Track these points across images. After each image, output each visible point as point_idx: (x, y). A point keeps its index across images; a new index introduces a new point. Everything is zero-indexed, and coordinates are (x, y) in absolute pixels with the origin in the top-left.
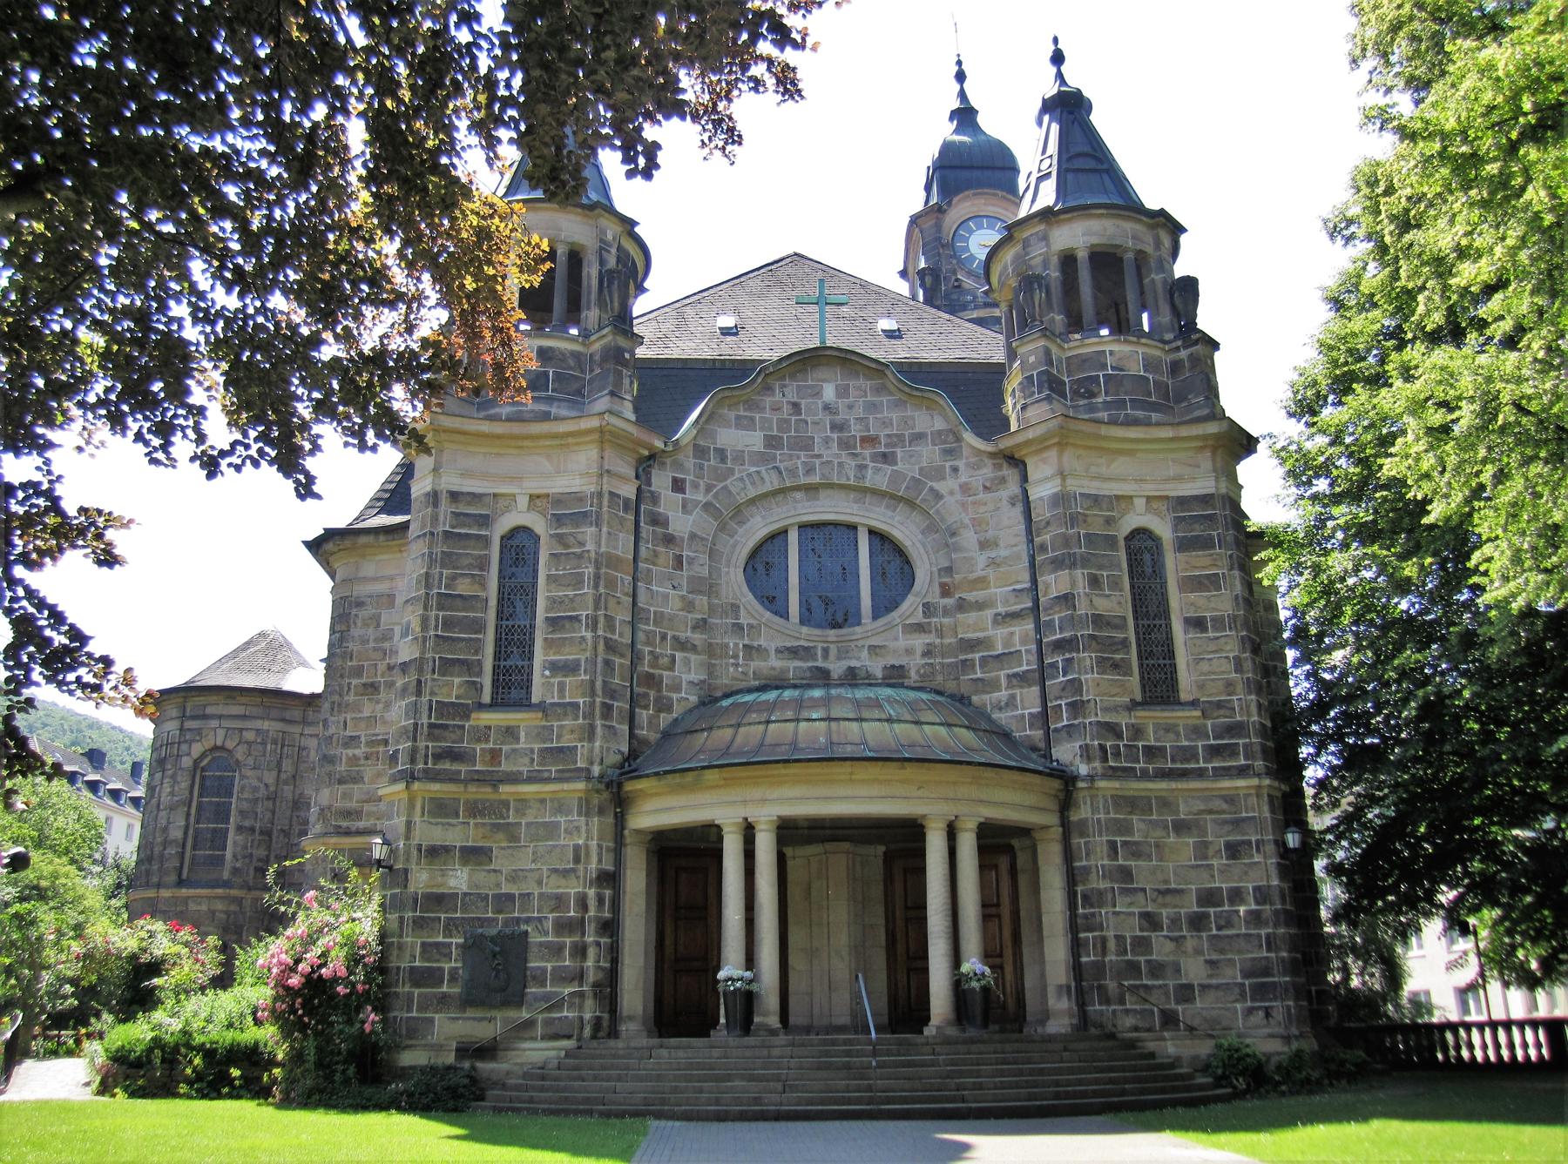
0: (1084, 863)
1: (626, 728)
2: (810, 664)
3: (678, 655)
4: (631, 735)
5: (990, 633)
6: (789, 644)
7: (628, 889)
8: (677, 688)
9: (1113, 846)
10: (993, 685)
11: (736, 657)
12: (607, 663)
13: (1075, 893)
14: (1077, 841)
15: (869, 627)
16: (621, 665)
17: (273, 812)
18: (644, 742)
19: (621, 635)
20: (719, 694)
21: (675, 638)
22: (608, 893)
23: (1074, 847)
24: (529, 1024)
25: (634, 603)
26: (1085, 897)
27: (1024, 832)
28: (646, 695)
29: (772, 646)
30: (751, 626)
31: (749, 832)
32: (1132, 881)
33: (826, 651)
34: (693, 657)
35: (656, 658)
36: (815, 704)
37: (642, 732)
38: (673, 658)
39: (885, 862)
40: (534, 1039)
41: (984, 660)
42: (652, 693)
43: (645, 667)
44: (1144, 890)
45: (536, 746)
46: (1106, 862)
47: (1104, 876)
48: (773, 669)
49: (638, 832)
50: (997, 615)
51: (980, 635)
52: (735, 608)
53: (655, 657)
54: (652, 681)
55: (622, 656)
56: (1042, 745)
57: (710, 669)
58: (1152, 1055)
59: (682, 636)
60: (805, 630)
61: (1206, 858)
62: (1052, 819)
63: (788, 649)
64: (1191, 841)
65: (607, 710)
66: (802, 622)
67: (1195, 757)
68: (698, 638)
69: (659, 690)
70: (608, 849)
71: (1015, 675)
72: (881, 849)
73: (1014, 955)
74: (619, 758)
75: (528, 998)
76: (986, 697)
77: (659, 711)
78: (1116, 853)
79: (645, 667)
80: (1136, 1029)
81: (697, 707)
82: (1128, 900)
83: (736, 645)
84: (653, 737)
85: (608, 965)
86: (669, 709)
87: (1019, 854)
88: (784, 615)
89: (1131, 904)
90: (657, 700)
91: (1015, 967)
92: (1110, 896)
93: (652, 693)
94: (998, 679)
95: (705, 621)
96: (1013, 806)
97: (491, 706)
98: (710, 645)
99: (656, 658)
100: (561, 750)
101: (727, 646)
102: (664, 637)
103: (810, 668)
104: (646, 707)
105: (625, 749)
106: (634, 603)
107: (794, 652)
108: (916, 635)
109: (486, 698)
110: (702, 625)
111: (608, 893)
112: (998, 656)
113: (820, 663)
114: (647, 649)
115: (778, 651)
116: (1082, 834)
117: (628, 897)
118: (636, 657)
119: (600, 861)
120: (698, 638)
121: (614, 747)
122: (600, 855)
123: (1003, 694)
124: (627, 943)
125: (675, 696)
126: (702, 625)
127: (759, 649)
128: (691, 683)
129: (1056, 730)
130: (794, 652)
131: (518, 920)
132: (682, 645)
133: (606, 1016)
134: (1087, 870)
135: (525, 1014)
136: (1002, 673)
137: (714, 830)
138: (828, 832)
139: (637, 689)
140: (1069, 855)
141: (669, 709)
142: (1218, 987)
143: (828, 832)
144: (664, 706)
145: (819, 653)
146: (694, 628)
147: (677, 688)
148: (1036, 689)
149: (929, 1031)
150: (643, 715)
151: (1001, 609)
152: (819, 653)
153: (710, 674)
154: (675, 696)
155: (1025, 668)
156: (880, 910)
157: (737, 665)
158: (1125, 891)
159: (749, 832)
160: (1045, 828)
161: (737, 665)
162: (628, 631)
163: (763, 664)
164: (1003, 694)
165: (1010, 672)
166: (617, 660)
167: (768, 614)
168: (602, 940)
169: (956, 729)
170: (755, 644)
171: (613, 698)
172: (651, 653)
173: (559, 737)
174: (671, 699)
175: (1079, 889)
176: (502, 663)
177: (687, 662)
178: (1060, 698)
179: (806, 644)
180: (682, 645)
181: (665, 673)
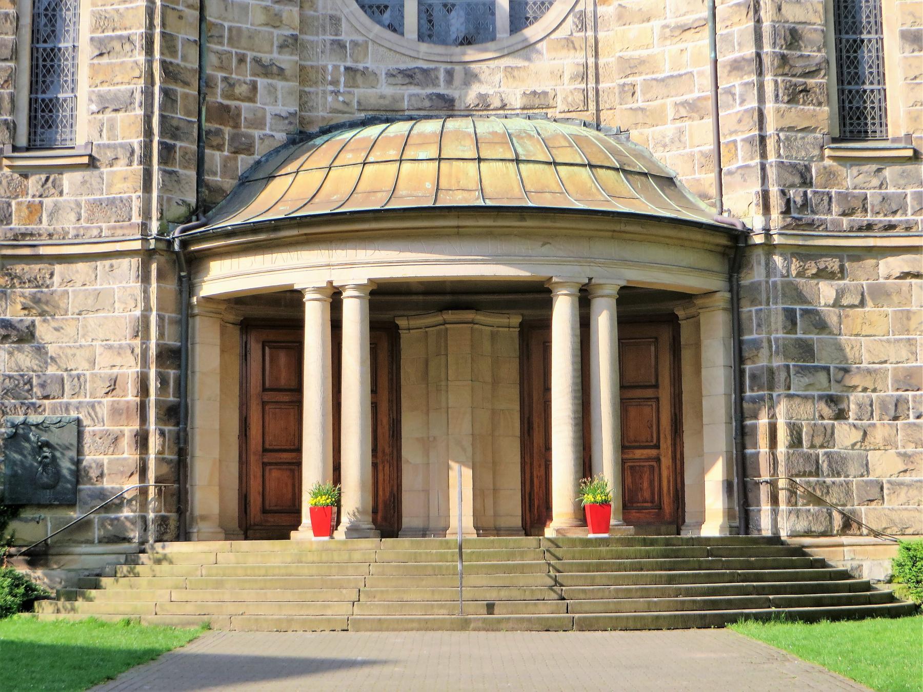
0: (755, 336)
1: (193, 174)
2: (429, 91)
3: (261, 82)
4: (200, 182)
5: (656, 50)
6: (402, 66)
7: (197, 369)
8: (258, 123)
9: (790, 315)
10: (657, 118)
11: (335, 82)
12: (167, 93)
13: (742, 373)
14: (748, 310)
15: (505, 43)
16: (186, 96)
17: (879, 449)
18: (217, 190)
19: (184, 58)
20: (314, 129)
21: (257, 61)
22: (172, 373)
23: (744, 316)
24: (84, 525)
25: (202, 18)
26: (754, 377)
27: (685, 297)
28: (218, 133)
29: (381, 69)
30: (355, 44)
31: (335, 298)
32: (813, 357)
33: (450, 74)
34: (280, 84)
35: (232, 86)
36: (424, 141)
37: (215, 179)
38: (254, 87)
39: (521, 333)
40: (91, 542)
41: (647, 84)
42: (227, 131)
43: (217, 97)
44: (827, 369)
45: (83, 199)
46: (780, 335)
47: (777, 353)
48: (382, 97)
49: (209, 299)
50: (665, 26)
51: (644, 53)
52: (335, 21)
53: (230, 84)
54: (226, 114)
55: (186, 84)
56: (713, 191)
57: (303, 100)
58: (822, 563)
59: (266, 57)
60: (424, 47)
61: (908, 331)
62: (716, 283)
63: (401, 72)
64: (890, 310)
65: (167, 151)
66: (421, 38)
67: (902, 208)
68: (287, 60)
69: (236, 126)
70: (172, 321)
71: (684, 104)
72: (516, 320)
73: (674, 445)
74: (183, 210)
75: (82, 495)
76: (648, 131)
77: (236, 152)
78: (794, 323)
79: (217, 97)
80: (808, 533)
81: (285, 146)
82: (806, 380)
83: (336, 67)
84: (228, 184)
85: (174, 457)
86: (248, 149)
87: (683, 323)
88: (396, 28)
89: (809, 386)
90: (233, 138)
91: (674, 458)
92: (783, 375)
93: (227, 131)
94: (663, 108)
95: (295, 38)
96: (664, 267)
97: (28, 149)
98: (302, 68)
99: (232, 86)
100: (112, 202)
101: (324, 68)
102: (242, 60)
103: (430, 97)
104: (219, 148)
105: (192, 199)
106: (202, 18)
107: (409, 76)
108: (564, 53)
109: (23, 141)
110: (292, 43)
111: (172, 373)
112: (663, 80)
113: (442, 90)
114: (220, 75)
115: (390, 75)
116: (753, 302)
117: (198, 376)
118: (205, 84)
119: (161, 335)
120: (287, 60)
121: (177, 197)
122: (161, 327)
123: (669, 129)
124: (197, 432)
125: (257, 133)
126: (292, 43)
127: (364, 72)
128: (278, 116)
129: (730, 173)
130: (409, 76)
131: (67, 407)
132: (266, 69)
133: (173, 516)
134: (756, 344)
135: (75, 515)
136: (669, 101)
137: (295, 295)
138: (448, 298)
139: (206, 125)
140: (737, 328)
141: (248, 149)
142: (909, 486)
143: (448, 298)
144: (243, 147)
145: (442, 75)
146: (281, 47)
147: (258, 123)
148: (709, 121)
149: (550, 532)
150: (215, 158)
151: (672, 22)
152: (442, 75)
153: (303, 105)
154: (257, 133)
155: (696, 94)
156: (515, 392)
157: (337, 93)
158: (802, 371)
159: (335, 298)
160: (709, 294)
161: (337, 93)
162: (194, 53)
163: (370, 91)
164: (669, 129)
165: (679, 99)
166: (180, 90)
167: (377, 28)
168: (167, 429)
169: (601, 172)
170: (360, 66)
171: (174, 137)
172: (225, 79)
173: (110, 186)
174: (250, 137)
175: (748, 367)
176: (40, 96)
177: (272, 90)
178: (736, 132)
179: (425, 66)
180: (266, 69)
181: (244, 105)
